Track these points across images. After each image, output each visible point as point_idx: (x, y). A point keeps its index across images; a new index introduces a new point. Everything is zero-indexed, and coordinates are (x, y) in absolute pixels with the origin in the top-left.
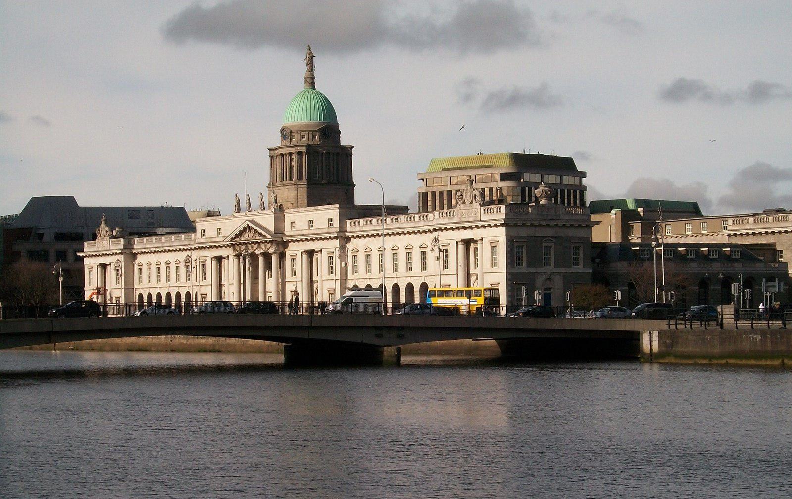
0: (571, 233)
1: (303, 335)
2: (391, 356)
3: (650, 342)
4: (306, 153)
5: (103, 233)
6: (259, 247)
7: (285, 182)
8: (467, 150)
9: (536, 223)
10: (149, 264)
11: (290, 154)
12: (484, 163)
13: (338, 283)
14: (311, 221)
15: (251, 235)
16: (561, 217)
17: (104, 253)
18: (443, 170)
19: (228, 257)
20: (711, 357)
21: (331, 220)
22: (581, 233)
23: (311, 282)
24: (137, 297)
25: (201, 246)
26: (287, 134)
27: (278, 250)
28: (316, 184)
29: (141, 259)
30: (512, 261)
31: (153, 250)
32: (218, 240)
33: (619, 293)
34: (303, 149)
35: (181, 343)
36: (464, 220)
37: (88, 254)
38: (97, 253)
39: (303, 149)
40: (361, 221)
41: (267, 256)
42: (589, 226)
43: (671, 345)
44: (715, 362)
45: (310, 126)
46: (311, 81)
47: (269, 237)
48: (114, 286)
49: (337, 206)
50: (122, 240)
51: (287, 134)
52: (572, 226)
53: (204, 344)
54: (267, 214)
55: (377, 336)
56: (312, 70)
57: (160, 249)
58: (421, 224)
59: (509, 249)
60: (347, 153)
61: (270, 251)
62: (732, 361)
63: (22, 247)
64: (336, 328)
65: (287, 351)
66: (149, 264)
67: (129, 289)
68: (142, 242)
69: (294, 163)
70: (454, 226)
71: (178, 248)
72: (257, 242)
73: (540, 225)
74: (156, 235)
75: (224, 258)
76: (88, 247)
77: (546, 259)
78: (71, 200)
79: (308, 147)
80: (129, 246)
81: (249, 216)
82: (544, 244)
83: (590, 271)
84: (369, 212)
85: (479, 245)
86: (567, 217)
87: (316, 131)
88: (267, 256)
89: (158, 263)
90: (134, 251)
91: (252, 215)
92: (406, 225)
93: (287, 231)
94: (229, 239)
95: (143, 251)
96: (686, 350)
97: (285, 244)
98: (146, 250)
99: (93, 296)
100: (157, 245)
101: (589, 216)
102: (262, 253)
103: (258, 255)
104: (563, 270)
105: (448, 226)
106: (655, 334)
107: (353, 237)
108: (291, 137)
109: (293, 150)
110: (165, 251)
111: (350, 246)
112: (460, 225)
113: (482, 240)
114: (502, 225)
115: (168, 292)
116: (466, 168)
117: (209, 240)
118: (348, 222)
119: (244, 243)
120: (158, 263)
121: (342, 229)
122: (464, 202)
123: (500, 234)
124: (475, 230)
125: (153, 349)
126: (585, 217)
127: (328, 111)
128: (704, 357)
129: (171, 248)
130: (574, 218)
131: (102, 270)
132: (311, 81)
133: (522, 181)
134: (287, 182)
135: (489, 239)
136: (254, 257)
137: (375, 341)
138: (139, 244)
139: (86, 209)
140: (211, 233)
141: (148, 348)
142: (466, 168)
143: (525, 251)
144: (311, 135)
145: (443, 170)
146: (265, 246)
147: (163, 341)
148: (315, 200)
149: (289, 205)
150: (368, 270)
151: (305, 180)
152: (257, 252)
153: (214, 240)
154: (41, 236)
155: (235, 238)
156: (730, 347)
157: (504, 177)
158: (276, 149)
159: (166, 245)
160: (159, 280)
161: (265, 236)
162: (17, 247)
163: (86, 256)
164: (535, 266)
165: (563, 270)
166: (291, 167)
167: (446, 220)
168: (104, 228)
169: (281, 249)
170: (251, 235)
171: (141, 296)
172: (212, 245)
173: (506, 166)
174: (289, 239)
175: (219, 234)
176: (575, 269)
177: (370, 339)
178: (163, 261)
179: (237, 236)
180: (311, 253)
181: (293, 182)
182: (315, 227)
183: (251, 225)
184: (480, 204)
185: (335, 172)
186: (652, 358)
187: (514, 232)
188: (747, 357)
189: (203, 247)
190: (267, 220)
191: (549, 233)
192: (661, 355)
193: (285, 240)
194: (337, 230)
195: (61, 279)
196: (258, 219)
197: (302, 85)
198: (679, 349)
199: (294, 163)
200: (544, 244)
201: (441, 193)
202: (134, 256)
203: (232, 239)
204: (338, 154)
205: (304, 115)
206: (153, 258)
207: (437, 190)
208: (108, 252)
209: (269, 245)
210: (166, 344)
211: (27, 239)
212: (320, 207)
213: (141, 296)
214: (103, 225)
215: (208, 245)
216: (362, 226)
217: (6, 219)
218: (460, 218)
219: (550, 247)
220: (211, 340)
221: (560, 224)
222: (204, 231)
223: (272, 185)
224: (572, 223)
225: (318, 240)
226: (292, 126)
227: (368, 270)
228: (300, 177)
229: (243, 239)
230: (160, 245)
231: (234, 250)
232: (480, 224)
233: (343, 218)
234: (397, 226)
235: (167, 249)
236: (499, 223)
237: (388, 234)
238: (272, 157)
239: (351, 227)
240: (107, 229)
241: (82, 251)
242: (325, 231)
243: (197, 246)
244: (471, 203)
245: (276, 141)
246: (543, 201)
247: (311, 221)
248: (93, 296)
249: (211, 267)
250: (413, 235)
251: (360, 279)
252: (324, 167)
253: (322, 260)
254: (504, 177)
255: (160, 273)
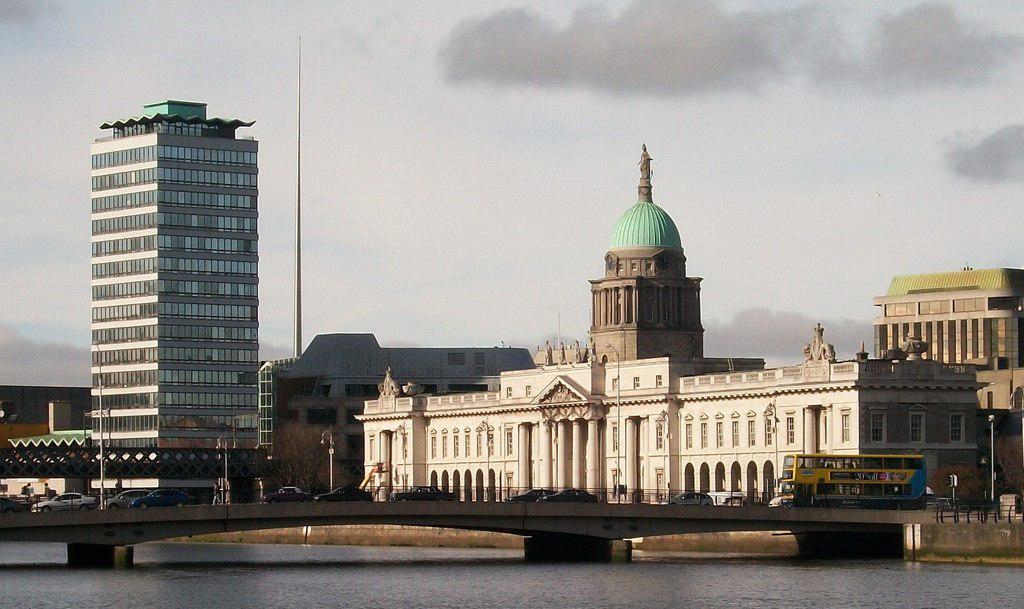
0: (948, 398)
1: (548, 527)
2: (619, 551)
3: (913, 537)
4: (636, 288)
5: (387, 389)
6: (573, 412)
7: (608, 326)
8: (947, 263)
9: (900, 385)
10: (704, 418)
11: (617, 289)
12: (967, 282)
13: (668, 459)
14: (637, 379)
15: (564, 395)
16: (936, 378)
17: (389, 416)
18: (910, 292)
19: (538, 423)
20: (966, 555)
21: (659, 377)
22: (963, 398)
23: (638, 459)
24: (430, 475)
25: (505, 408)
26: (613, 262)
27: (596, 416)
28: (650, 329)
29: (434, 424)
30: (868, 433)
31: (449, 413)
32: (527, 401)
33: (956, 477)
34: (633, 283)
35: (451, 537)
36: (811, 380)
37: (368, 417)
38: (380, 417)
39: (633, 283)
40: (697, 379)
41: (583, 424)
42: (974, 389)
43: (933, 540)
44: (971, 560)
45: (643, 251)
46: (646, 192)
47: (584, 398)
48: (653, 450)
49: (667, 359)
50: (411, 399)
51: (613, 262)
52: (950, 389)
53: (477, 538)
54: (584, 368)
55: (606, 527)
56: (648, 177)
57: (458, 412)
58: (766, 384)
59: (863, 419)
60: (694, 286)
61: (586, 417)
62: (985, 560)
63: (302, 405)
64: (556, 518)
65: (528, 545)
66: (445, 432)
67: (419, 465)
68: (434, 403)
69: (621, 301)
70: (799, 388)
71: (479, 411)
72: (571, 406)
73: (905, 388)
74: (484, 388)
75: (643, 419)
76: (370, 408)
77: (954, 431)
78: (368, 340)
79: (639, 279)
80: (419, 407)
81: (561, 370)
82: (911, 413)
83: (975, 447)
84: (718, 367)
85: (828, 414)
86: (943, 378)
87: (650, 259)
88: (583, 424)
89: (456, 431)
90: (426, 414)
91: (565, 370)
92: (748, 386)
93: (609, 391)
94: (537, 401)
95: (437, 414)
96: (945, 546)
97: (606, 408)
98: (441, 414)
99: (374, 474)
100: (454, 407)
101: (974, 376)
102: (577, 420)
103: (572, 422)
104: (936, 446)
105: (793, 389)
106: (918, 527)
107: (686, 400)
108: (618, 267)
109: (619, 284)
110: (464, 415)
111: (683, 412)
112: (806, 388)
113: (831, 406)
114: (853, 388)
115: (704, 463)
116: (941, 290)
117: (516, 401)
118: (682, 380)
119: (555, 407)
120: (456, 431)
121: (673, 389)
122: (812, 358)
123: (852, 400)
124: (824, 394)
125: (418, 544)
126: (968, 378)
127: (668, 230)
128: (961, 555)
129: (470, 412)
130: (953, 378)
131: (386, 440)
132: (646, 192)
133: (1020, 309)
134: (613, 326)
135: (840, 406)
136: (567, 423)
137: (606, 534)
138: (434, 404)
139: (388, 350)
140: (519, 392)
141: (413, 542)
142: (941, 290)
143: (884, 421)
144: (643, 264)
145: (910, 292)
146: (581, 411)
147: (430, 534)
148: (645, 351)
149: (615, 357)
150: (704, 444)
151: (634, 324)
152: (571, 418)
153: (522, 401)
154: (327, 389)
155: (544, 400)
156: (983, 544)
157: (994, 303)
158: (600, 282)
159: (465, 406)
160: (456, 454)
161: (580, 398)
162: (292, 405)
163: (366, 420)
164: (898, 441)
165: (936, 446)
166: (618, 307)
167: (791, 381)
168: (389, 383)
169: (601, 415)
170: (564, 395)
171: (434, 474)
172: (519, 407)
173: (997, 288)
174: (610, 401)
175: (528, 393)
176: (954, 445)
177: (596, 531)
178: (462, 429)
179: (547, 397)
180: (637, 421)
181: (619, 325)
182: (641, 386)
183: (563, 382)
184: (829, 361)
185: (676, 313)
186: (915, 555)
187: (871, 397)
188: (999, 556)
189: (508, 411)
190: (583, 376)
191: (920, 397)
192: (923, 552)
193: (605, 402)
194: (667, 391)
195: (331, 451)
196: (573, 375)
197: (634, 197)
198: (939, 545)
199: (621, 301)
200: (911, 413)
201: (975, 322)
202: (427, 420)
203: (541, 401)
204: (680, 288)
205: (635, 238)
206: (449, 424)
207: (900, 321)
208: (393, 416)
209: (585, 410)
210: (434, 538)
211: (308, 392)
212: (647, 360)
213: (434, 474)
214: (388, 379)
215: (514, 408)
216: (709, 384)
217: (281, 365)
218: (808, 378)
219: (920, 416)
220: (429, 531)
221: (933, 386)
222: (510, 389)
223: (594, 328)
224: (949, 385)
225: (645, 404)
226: (620, 252)
227: (704, 444)
228: (629, 321)
229: (554, 401)
230: (459, 407)
231: (544, 415)
232: (828, 386)
233: (674, 374)
234: (755, 385)
235: (466, 412)
236: (849, 385)
237: (624, 403)
238: (594, 292)
239: (687, 387)
240: (392, 384)
241: (362, 414)
242: (653, 392)
243: (500, 409)
244: (820, 359)
245: (600, 271)
246: (910, 358)
247: (637, 379)
248: (374, 474)
249: (519, 436)
250: (756, 399)
251: (694, 456)
252: (661, 307)
253: (648, 431)
254: (994, 303)
255: (792, 427)
